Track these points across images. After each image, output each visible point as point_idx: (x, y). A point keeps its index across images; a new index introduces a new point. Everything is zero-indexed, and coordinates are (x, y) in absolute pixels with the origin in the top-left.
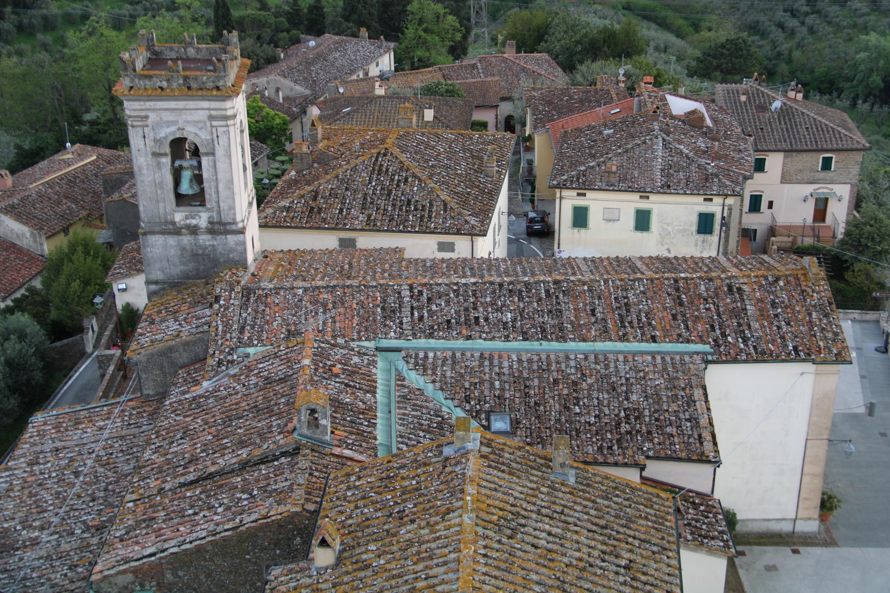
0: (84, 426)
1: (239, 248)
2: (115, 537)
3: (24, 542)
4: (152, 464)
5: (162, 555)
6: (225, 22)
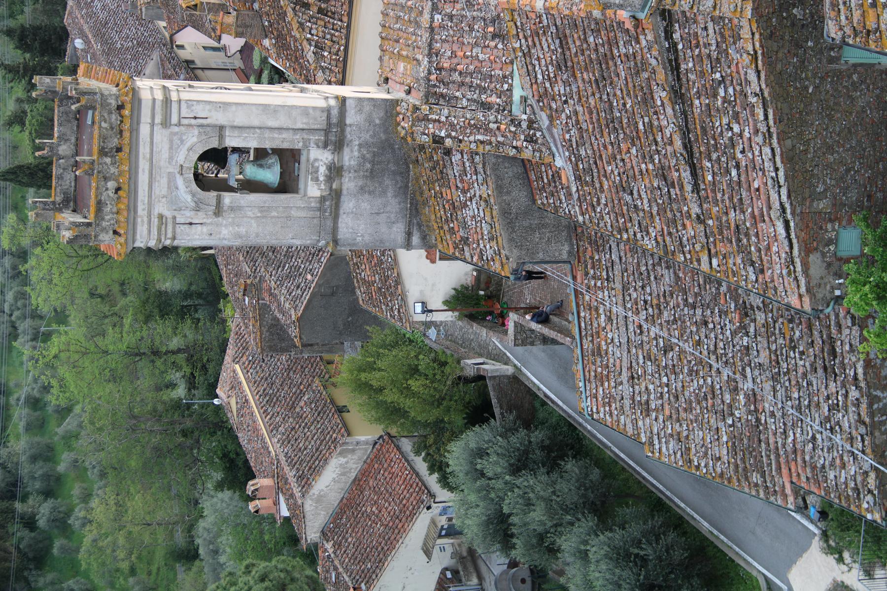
0: (603, 343)
1: (367, 108)
2: (757, 281)
3: (750, 412)
4: (663, 235)
5: (788, 211)
6: (41, 174)
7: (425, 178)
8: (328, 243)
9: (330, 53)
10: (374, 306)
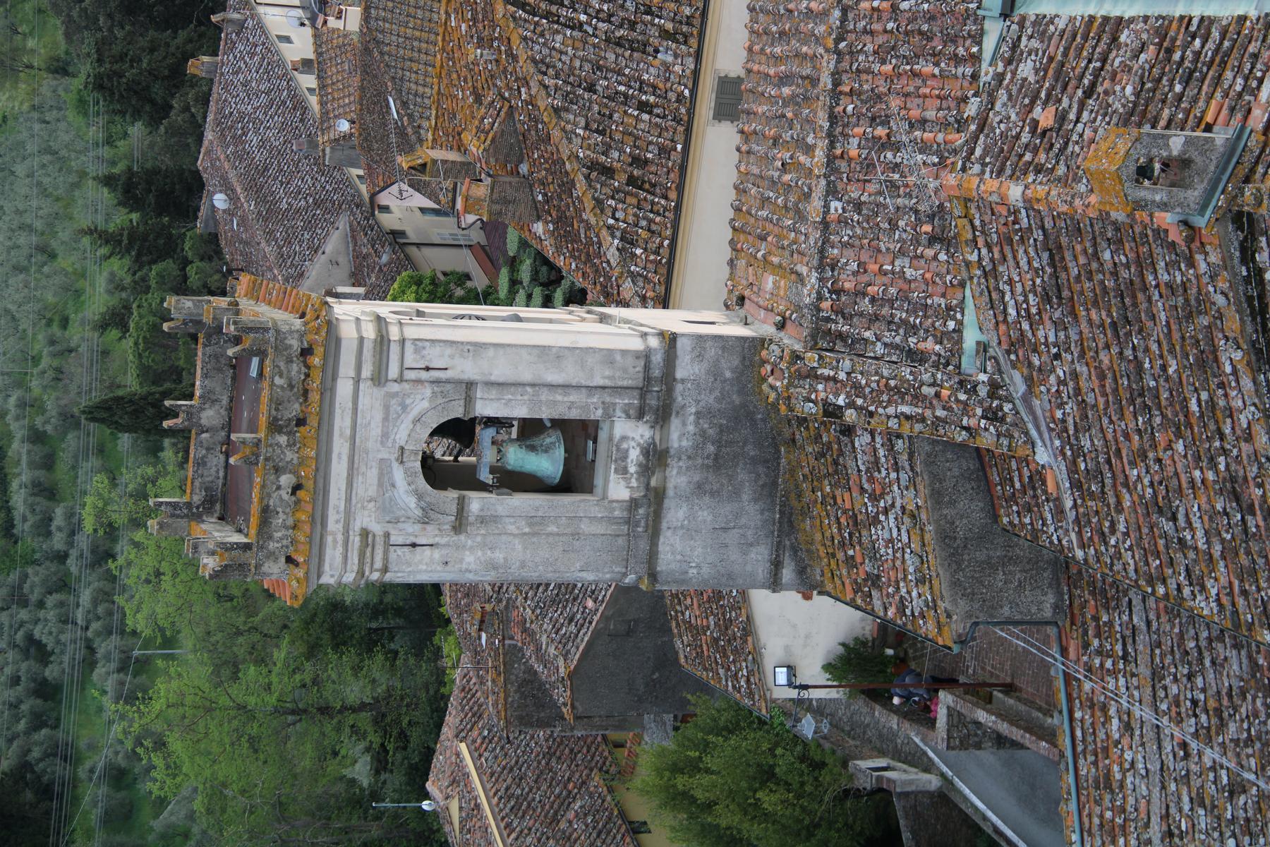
0: (1116, 768)
1: (712, 352)
4: (1231, 594)
7: (806, 470)
8: (640, 578)
9: (645, 250)
10: (705, 669)
